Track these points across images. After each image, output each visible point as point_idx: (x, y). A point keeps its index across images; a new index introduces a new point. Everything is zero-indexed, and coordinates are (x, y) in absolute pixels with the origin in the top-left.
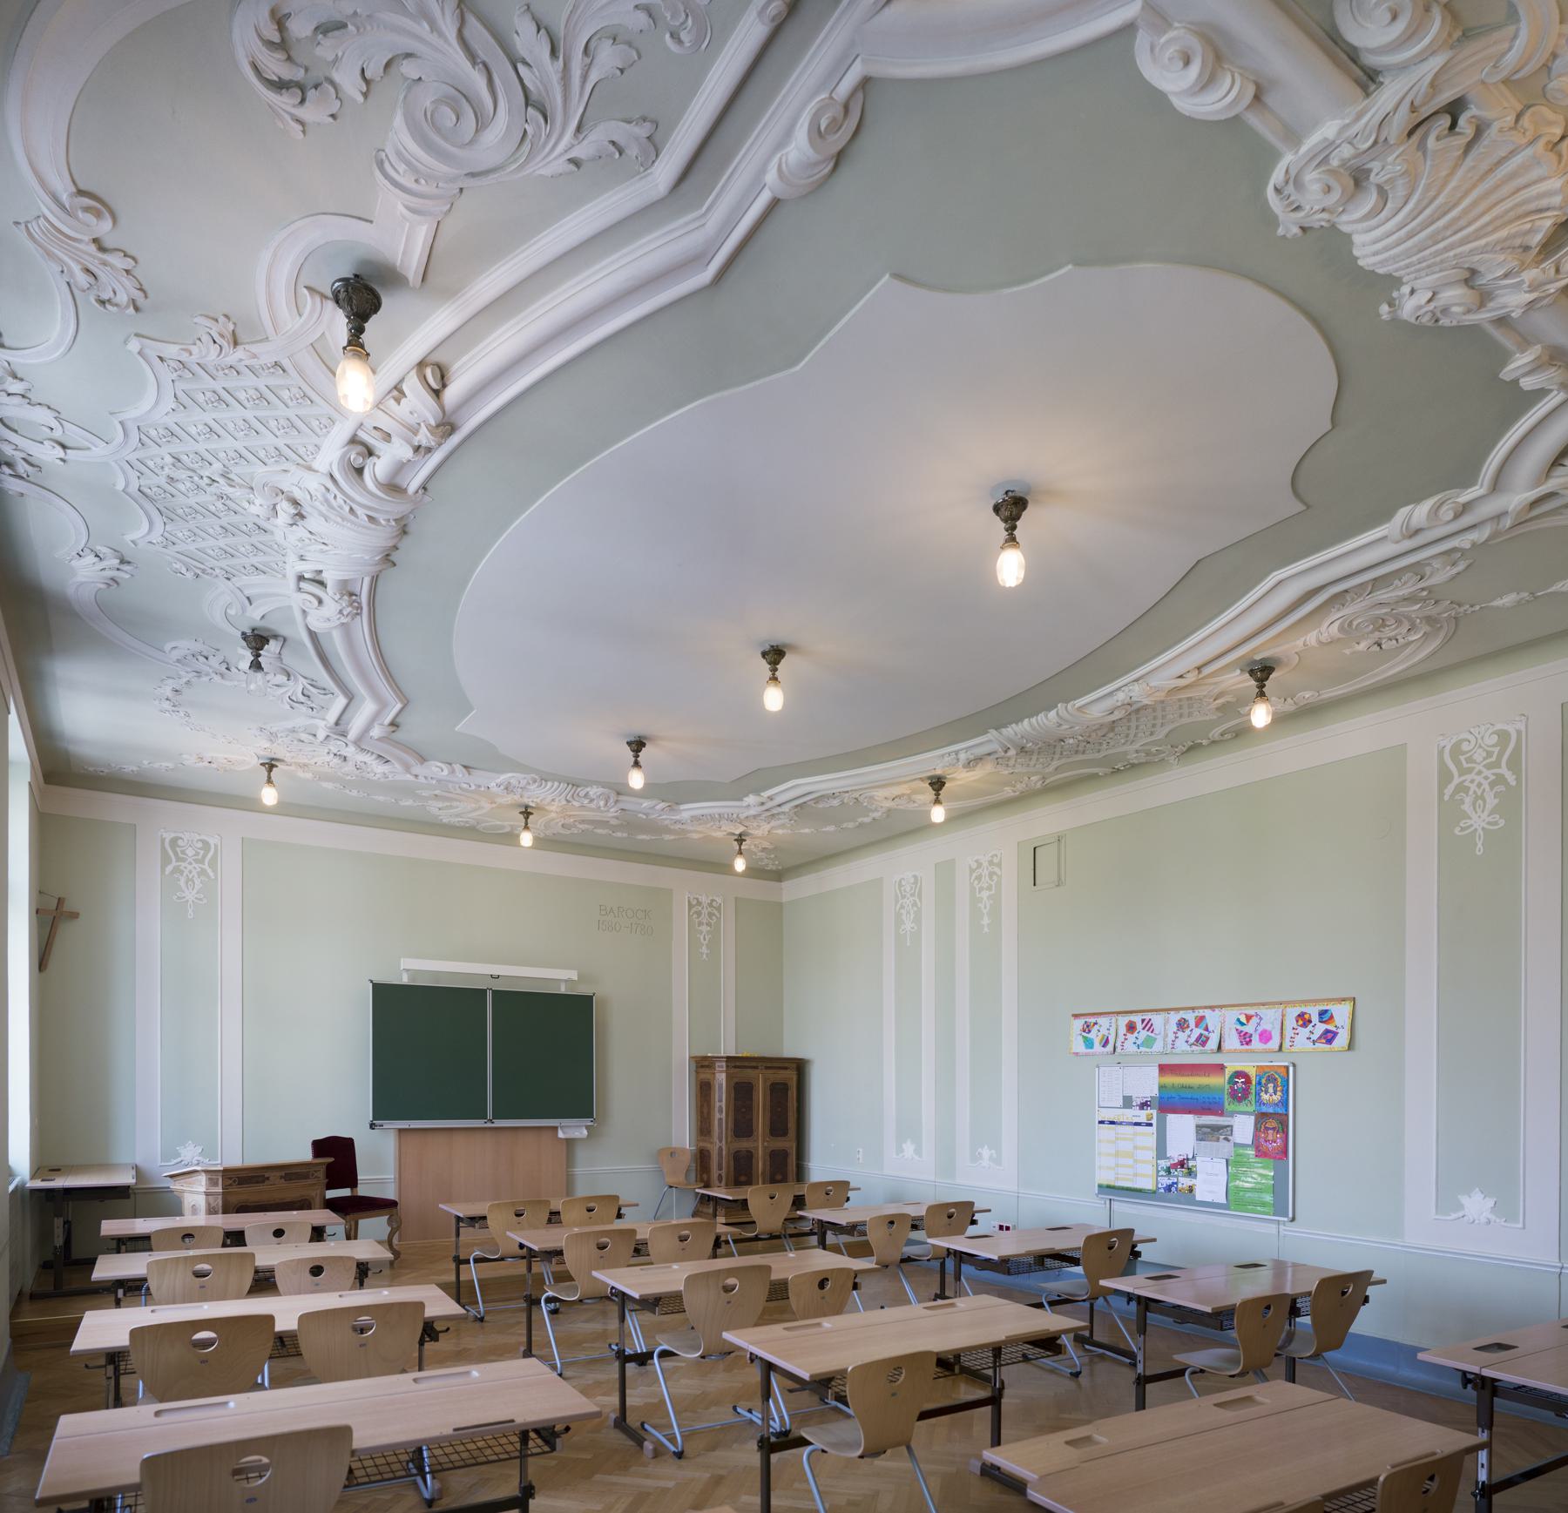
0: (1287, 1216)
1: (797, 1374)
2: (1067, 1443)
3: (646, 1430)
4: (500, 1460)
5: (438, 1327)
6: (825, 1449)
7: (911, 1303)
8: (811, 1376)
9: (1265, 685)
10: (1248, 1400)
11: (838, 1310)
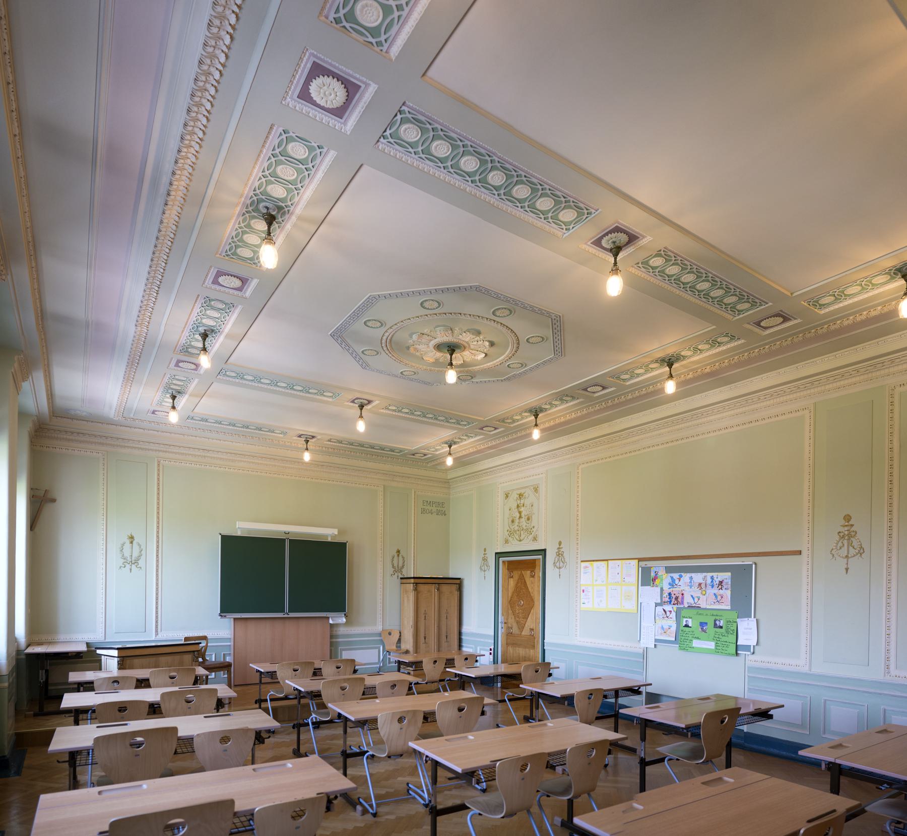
0: (750, 651)
1: (449, 766)
2: (703, 783)
4: (239, 832)
5: (264, 735)
6: (481, 813)
7: (517, 724)
8: (463, 770)
10: (720, 779)
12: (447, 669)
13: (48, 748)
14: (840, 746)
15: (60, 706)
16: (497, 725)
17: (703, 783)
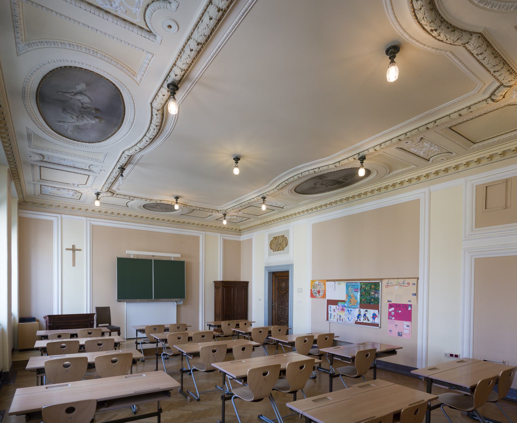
0: (378, 327)
2: (359, 387)
3: (189, 393)
8: (236, 377)
9: (363, 162)
11: (249, 357)
12: (269, 337)
13: (26, 367)
14: (434, 369)
17: (359, 387)
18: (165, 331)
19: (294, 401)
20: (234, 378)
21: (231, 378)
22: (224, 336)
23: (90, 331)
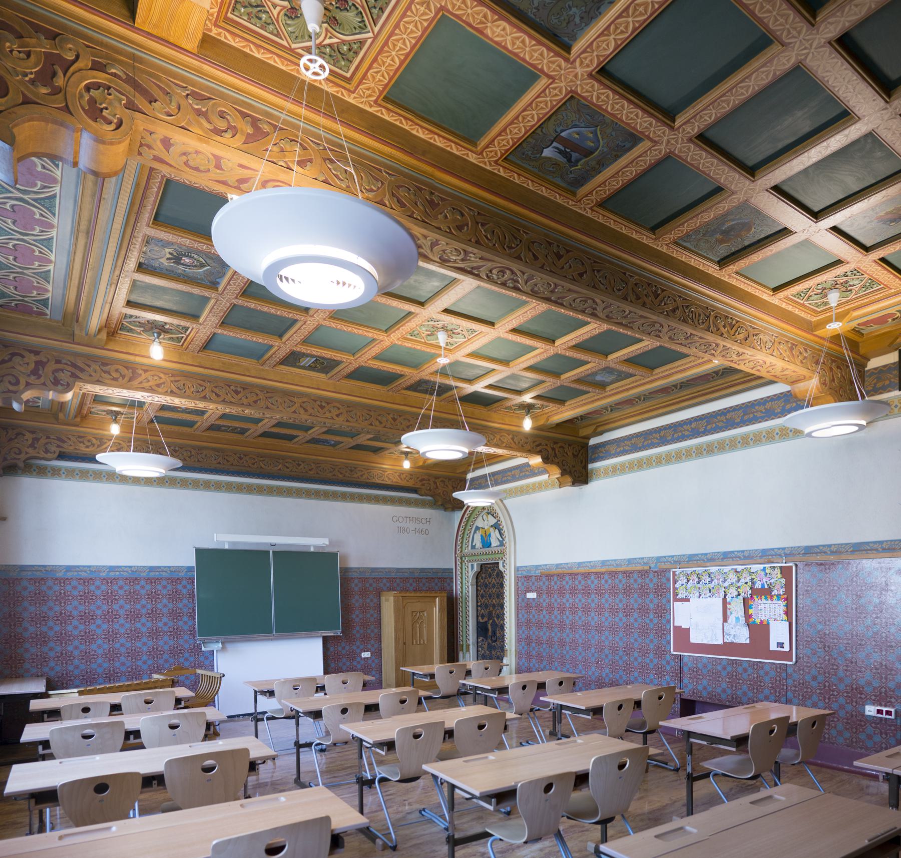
8: (481, 793)
10: (770, 797)
15: (4, 790)
16: (521, 744)
18: (317, 691)
19: (688, 815)
20: (474, 797)
21: (468, 796)
22: (442, 697)
23: (149, 698)
